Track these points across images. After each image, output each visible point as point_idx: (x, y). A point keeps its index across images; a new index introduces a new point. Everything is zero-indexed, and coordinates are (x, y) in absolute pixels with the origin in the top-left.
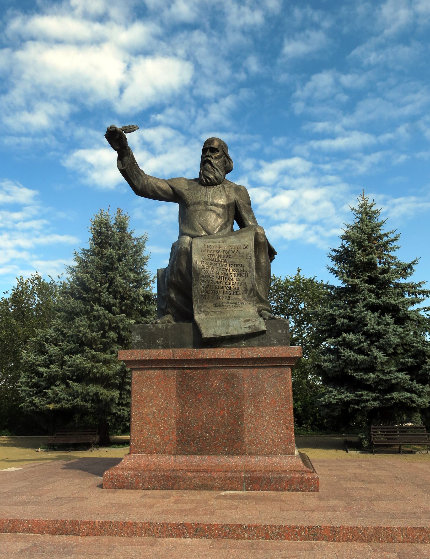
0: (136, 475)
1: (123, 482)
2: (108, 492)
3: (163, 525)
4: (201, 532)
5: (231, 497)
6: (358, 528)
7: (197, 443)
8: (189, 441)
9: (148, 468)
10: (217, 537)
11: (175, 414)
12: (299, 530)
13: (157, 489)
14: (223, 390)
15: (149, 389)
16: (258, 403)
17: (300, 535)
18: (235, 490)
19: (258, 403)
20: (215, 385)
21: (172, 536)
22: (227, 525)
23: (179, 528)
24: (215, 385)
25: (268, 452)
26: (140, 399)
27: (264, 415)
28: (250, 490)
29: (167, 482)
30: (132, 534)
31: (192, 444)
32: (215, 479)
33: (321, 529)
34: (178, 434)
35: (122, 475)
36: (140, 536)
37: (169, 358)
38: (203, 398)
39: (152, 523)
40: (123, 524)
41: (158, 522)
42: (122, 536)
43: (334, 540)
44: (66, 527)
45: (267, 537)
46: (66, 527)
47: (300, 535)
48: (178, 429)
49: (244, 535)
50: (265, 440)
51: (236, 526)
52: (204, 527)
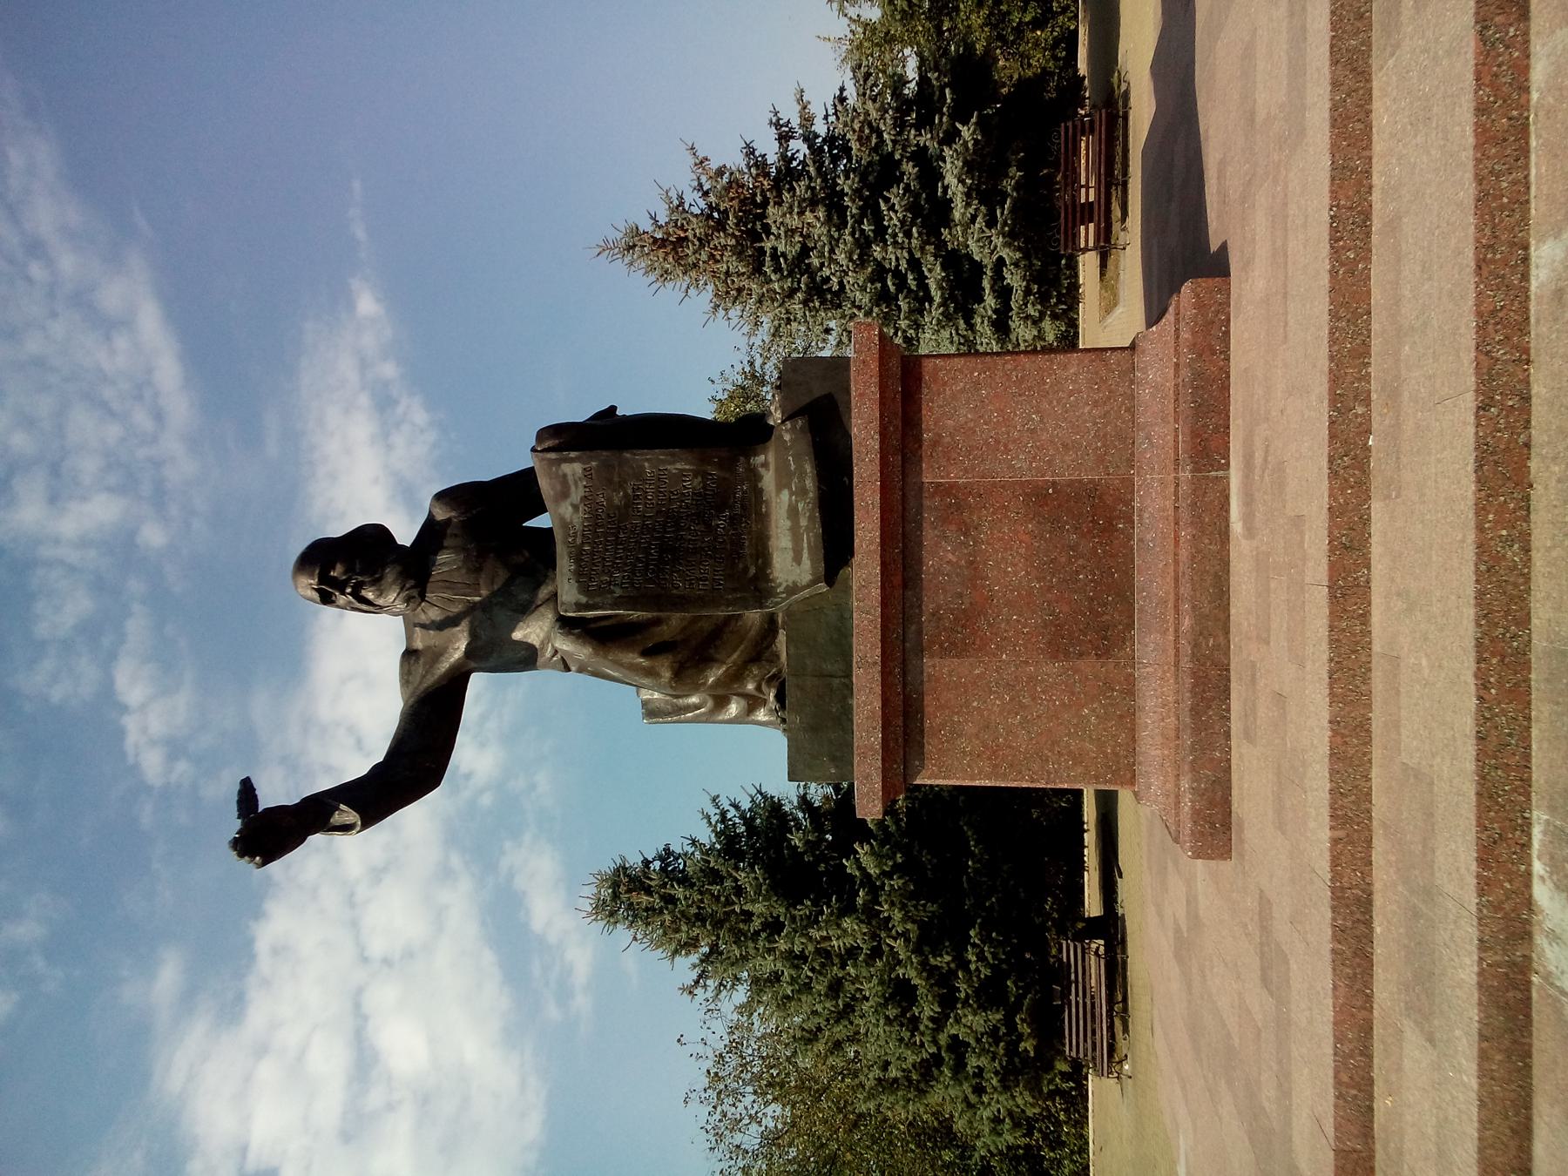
0: (1193, 769)
1: (1212, 804)
2: (1242, 841)
3: (1334, 643)
4: (1353, 534)
5: (1249, 501)
6: (1334, 108)
7: (1105, 605)
8: (1096, 623)
9: (1172, 734)
10: (1363, 490)
11: (1026, 662)
12: (1342, 265)
13: (1228, 710)
14: (965, 535)
15: (960, 736)
16: (997, 442)
17: (1355, 261)
18: (1227, 497)
19: (997, 442)
20: (950, 556)
21: (1365, 618)
22: (1331, 461)
23: (1344, 595)
24: (950, 556)
25: (1128, 417)
26: (989, 758)
27: (1030, 425)
28: (1227, 457)
29: (1210, 685)
30: (1362, 729)
31: (1106, 617)
32: (1198, 552)
33: (1337, 206)
34: (1081, 655)
35: (1193, 807)
36: (1369, 706)
37: (878, 677)
38: (983, 587)
39: (1331, 674)
40: (1335, 756)
41: (1325, 657)
42: (1370, 761)
43: (1368, 173)
44: (1349, 924)
45: (1362, 353)
46: (1349, 924)
47: (1355, 261)
48: (1067, 655)
49: (1356, 416)
50: (1095, 424)
51: (1332, 436)
52: (1339, 527)
